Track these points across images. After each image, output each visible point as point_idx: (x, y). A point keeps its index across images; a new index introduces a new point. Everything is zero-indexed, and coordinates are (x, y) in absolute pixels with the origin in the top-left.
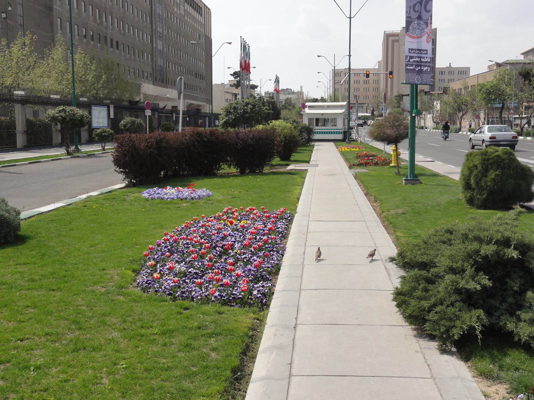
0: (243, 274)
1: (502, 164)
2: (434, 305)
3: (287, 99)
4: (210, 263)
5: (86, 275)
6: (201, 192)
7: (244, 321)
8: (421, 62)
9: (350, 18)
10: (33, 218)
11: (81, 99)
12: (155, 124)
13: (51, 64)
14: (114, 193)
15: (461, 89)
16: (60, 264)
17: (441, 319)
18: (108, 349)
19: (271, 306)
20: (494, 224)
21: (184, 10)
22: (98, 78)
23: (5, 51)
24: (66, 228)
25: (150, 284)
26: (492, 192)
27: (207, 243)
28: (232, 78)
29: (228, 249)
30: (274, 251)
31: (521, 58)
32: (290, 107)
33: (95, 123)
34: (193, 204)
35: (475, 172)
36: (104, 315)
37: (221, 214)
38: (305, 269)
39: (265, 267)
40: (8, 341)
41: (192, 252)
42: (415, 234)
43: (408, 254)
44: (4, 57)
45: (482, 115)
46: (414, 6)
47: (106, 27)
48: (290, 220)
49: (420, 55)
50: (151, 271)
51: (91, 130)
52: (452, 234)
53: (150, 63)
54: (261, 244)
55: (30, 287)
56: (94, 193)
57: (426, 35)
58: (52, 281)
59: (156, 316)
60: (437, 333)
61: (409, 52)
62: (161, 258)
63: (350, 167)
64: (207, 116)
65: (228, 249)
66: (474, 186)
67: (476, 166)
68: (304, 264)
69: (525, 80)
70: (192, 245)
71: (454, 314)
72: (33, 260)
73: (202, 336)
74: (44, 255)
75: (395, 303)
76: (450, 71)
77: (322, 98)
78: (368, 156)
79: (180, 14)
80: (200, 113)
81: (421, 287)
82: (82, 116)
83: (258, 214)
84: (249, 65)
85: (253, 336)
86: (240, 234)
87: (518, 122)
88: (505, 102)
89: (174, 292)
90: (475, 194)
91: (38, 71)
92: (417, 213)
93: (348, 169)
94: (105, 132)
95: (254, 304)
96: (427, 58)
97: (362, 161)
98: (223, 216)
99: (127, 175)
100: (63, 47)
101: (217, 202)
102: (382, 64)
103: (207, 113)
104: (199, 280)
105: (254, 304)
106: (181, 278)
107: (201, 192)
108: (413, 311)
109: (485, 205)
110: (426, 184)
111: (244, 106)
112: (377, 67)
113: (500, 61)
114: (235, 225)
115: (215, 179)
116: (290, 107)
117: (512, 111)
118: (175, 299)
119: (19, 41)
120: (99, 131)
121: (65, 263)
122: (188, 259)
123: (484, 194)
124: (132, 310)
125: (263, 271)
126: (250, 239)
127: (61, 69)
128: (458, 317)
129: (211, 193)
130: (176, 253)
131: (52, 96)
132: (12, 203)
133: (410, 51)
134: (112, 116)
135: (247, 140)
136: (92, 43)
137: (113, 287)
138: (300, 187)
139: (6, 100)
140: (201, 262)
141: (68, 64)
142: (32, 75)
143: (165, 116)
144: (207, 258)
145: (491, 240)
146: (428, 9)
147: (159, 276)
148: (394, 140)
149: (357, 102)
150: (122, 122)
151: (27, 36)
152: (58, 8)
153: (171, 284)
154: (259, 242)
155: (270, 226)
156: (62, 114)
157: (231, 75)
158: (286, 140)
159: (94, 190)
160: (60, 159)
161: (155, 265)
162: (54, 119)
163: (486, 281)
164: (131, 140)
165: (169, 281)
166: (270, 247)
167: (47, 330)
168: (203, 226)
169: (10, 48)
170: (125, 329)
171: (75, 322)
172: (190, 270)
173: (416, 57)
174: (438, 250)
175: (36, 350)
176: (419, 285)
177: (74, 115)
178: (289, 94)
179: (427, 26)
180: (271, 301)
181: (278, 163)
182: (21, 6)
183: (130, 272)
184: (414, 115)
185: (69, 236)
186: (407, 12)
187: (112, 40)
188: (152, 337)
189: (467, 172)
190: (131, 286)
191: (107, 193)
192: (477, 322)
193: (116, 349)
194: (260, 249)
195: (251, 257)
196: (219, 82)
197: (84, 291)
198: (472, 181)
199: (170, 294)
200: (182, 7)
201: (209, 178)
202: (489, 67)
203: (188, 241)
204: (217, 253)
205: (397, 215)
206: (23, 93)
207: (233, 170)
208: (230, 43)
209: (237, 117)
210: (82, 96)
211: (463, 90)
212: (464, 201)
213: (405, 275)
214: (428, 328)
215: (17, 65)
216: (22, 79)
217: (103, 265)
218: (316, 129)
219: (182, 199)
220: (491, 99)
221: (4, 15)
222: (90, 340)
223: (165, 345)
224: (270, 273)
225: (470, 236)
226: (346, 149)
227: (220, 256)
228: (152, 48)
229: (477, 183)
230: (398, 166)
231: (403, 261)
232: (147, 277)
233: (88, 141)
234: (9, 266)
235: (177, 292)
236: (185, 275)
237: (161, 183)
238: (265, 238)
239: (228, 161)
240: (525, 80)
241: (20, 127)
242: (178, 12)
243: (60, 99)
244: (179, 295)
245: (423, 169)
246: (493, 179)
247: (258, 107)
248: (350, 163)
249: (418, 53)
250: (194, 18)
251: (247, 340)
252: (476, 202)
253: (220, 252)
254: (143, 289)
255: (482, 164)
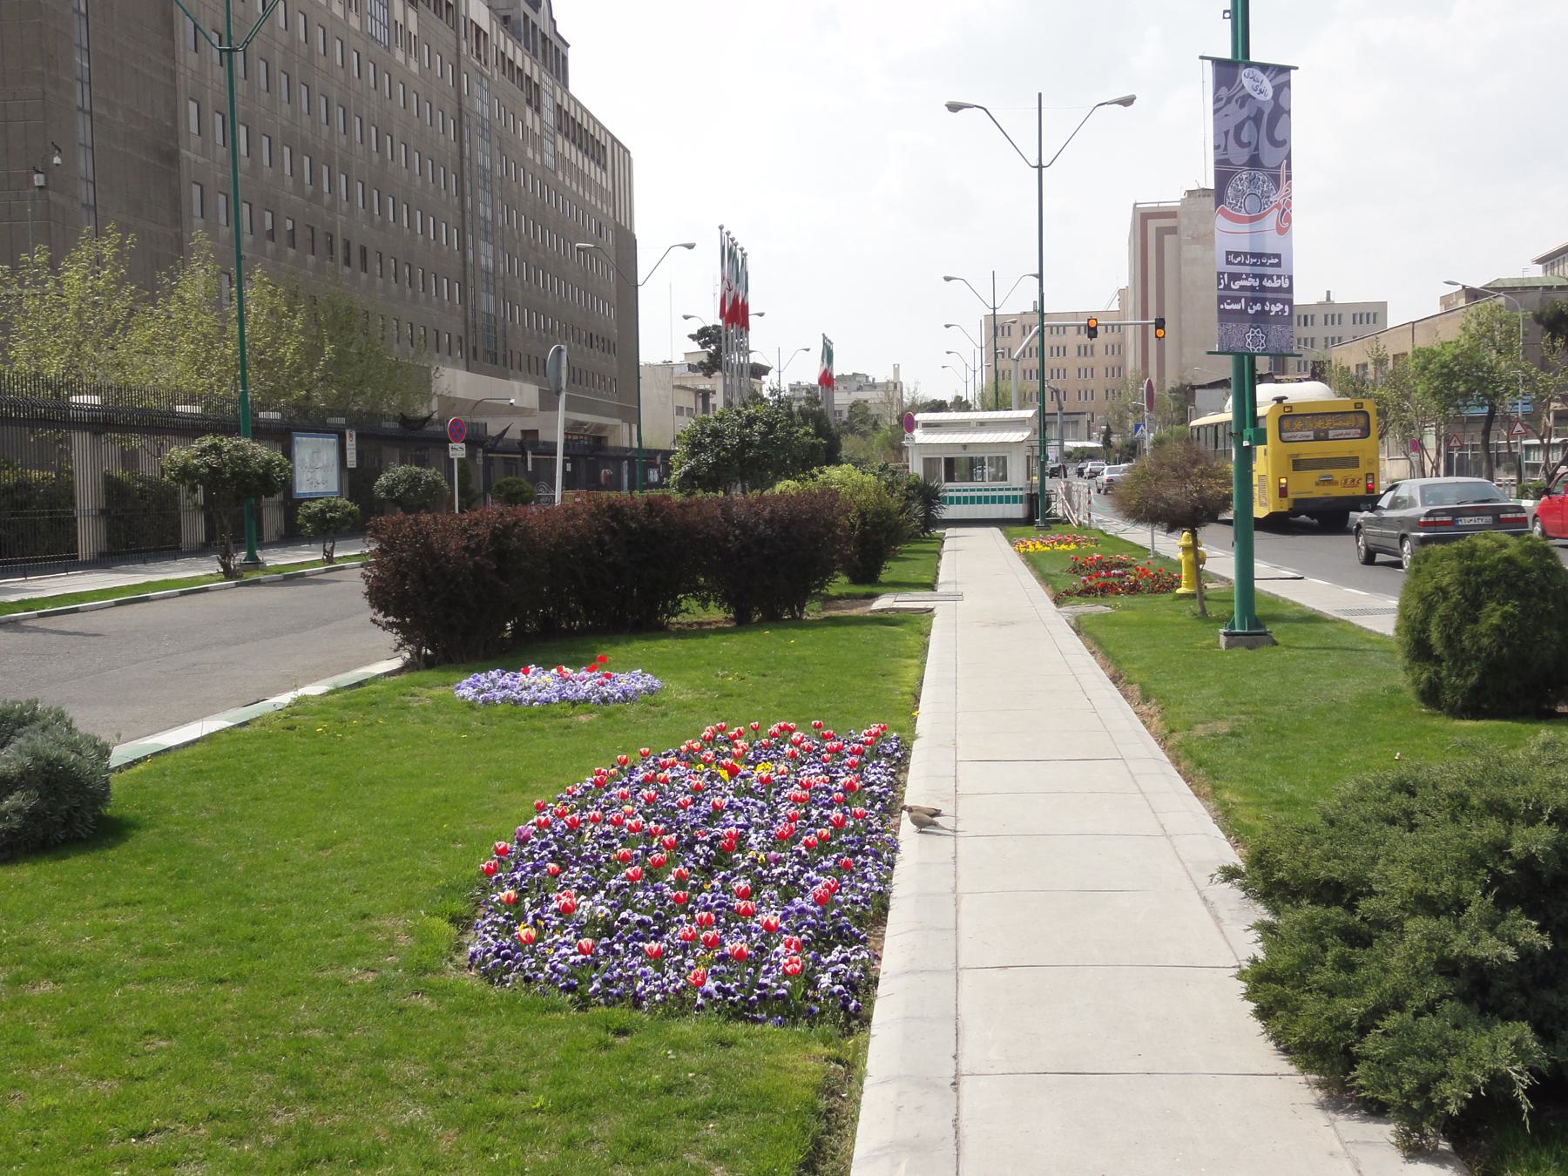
0: (783, 925)
1: (1521, 583)
2: (1378, 1012)
3: (854, 405)
4: (681, 894)
5: (316, 934)
6: (632, 680)
7: (801, 1065)
8: (1263, 288)
9: (1040, 167)
10: (140, 767)
11: (262, 415)
12: (477, 484)
13: (177, 316)
14: (372, 687)
15: (1365, 366)
16: (233, 902)
17: (1404, 1053)
18: (402, 1157)
19: (875, 1020)
20: (1534, 761)
21: (556, 155)
22: (311, 353)
23: (46, 281)
24: (240, 794)
25: (506, 957)
26: (1494, 667)
27: (664, 833)
28: (695, 347)
29: (730, 848)
30: (865, 854)
31: (1537, 272)
32: (864, 428)
33: (305, 484)
34: (608, 715)
35: (1442, 609)
36: (380, 1054)
37: (696, 745)
38: (964, 905)
39: (845, 902)
40: (101, 1138)
41: (625, 858)
42: (1275, 796)
43: (1283, 856)
44: (42, 300)
45: (1430, 441)
46: (1239, 128)
47: (332, 208)
48: (899, 760)
49: (1258, 270)
50: (508, 918)
51: (292, 503)
52: (1413, 794)
53: (459, 308)
54: (825, 832)
55: (151, 973)
56: (314, 690)
57: (1275, 213)
58: (215, 955)
59: (533, 1055)
60: (1393, 1096)
61: (1228, 263)
62: (532, 881)
63: (1058, 600)
64: (624, 458)
65: (730, 848)
66: (1439, 650)
67: (1443, 592)
68: (960, 890)
69: (1553, 338)
70: (622, 840)
71: (1439, 1036)
72: (153, 891)
73: (680, 1114)
74: (182, 875)
75: (1252, 1006)
76: (1331, 313)
77: (958, 399)
78: (1108, 567)
79: (543, 166)
80: (604, 448)
81: (1330, 956)
82: (269, 462)
83: (806, 744)
84: (745, 308)
85: (830, 1111)
86: (760, 803)
87: (1537, 458)
88: (1497, 402)
89: (581, 983)
90: (1444, 673)
91: (139, 337)
92: (1275, 731)
93: (1053, 606)
94: (334, 508)
95: (822, 1013)
96: (1279, 277)
97: (1090, 580)
98: (701, 750)
99: (409, 634)
100: (209, 267)
101: (678, 709)
102: (1131, 299)
103: (626, 450)
104: (654, 945)
105: (822, 1013)
106: (597, 938)
107: (632, 680)
108: (1314, 1030)
109: (1474, 707)
110: (1289, 647)
111: (742, 427)
112: (1115, 307)
113: (1477, 284)
114: (743, 777)
115: (666, 641)
116: (864, 428)
117: (1519, 427)
118: (584, 1004)
119: (84, 253)
120: (316, 506)
121: (249, 900)
122: (612, 882)
123: (1469, 674)
124: (461, 1041)
125: (840, 915)
126: (792, 819)
127: (204, 329)
128: (1454, 1049)
129: (657, 683)
130: (576, 864)
131: (179, 408)
132: (87, 721)
133: (1231, 258)
134: (352, 461)
135: (756, 525)
136: (291, 252)
137: (396, 969)
138: (915, 661)
139: (46, 422)
140: (655, 889)
141: (224, 317)
142: (122, 350)
143: (508, 461)
144: (671, 878)
145: (1539, 810)
146: (1278, 136)
147: (533, 933)
148: (1189, 518)
149: (1061, 408)
150: (382, 479)
151: (108, 236)
152: (193, 157)
153: (572, 959)
154: (818, 826)
155: (848, 779)
156: (211, 459)
157: (691, 336)
158: (864, 523)
159: (310, 680)
160: (206, 590)
161: (517, 902)
162: (186, 473)
163: (1532, 935)
164: (420, 531)
165: (564, 950)
166: (852, 842)
167: (212, 1102)
168: (647, 781)
169: (58, 274)
170: (445, 1096)
171: (296, 1079)
172: (624, 915)
173: (1248, 275)
174: (1376, 844)
175: (187, 1164)
176: (1325, 949)
177: (245, 460)
178: (860, 389)
179: (1278, 187)
180: (871, 1003)
181: (844, 591)
182: (89, 151)
183: (442, 926)
184: (1246, 443)
185: (251, 817)
186: (1216, 147)
187: (347, 246)
188: (529, 1121)
189: (1416, 610)
190: (450, 966)
191: (351, 687)
192: (1513, 1062)
193: (425, 1157)
194: (824, 846)
195: (801, 872)
196: (656, 359)
197: (313, 983)
198: (1435, 636)
199: (570, 989)
200: (548, 146)
201: (647, 639)
202: (1445, 300)
203: (608, 828)
204: (697, 862)
205: (1217, 740)
206: (96, 400)
207: (716, 614)
208: (690, 247)
209: (723, 459)
210: (267, 408)
211: (1371, 368)
212: (1410, 694)
213: (1268, 918)
214: (1363, 1082)
215: (80, 319)
216: (93, 360)
217: (362, 903)
218: (950, 488)
219: (574, 704)
220: (1457, 394)
221: (39, 180)
222: (343, 1131)
223: (570, 1143)
224: (859, 920)
225: (1474, 801)
226: (1038, 546)
227: (708, 872)
228: (465, 265)
229: (1449, 641)
230: (1201, 593)
231: (1267, 879)
232: (495, 938)
233: (282, 537)
234: (82, 909)
235: (591, 981)
236: (609, 930)
237: (512, 655)
238: (836, 813)
239: (700, 588)
240: (1553, 338)
241: (87, 498)
242: (538, 160)
243: (203, 417)
244: (596, 990)
245: (1274, 600)
246: (1498, 629)
247: (782, 428)
248: (1054, 588)
249: (1254, 264)
250: (582, 177)
251: (819, 1126)
252: (1448, 696)
253: (707, 858)
254: (485, 973)
255: (1462, 584)
